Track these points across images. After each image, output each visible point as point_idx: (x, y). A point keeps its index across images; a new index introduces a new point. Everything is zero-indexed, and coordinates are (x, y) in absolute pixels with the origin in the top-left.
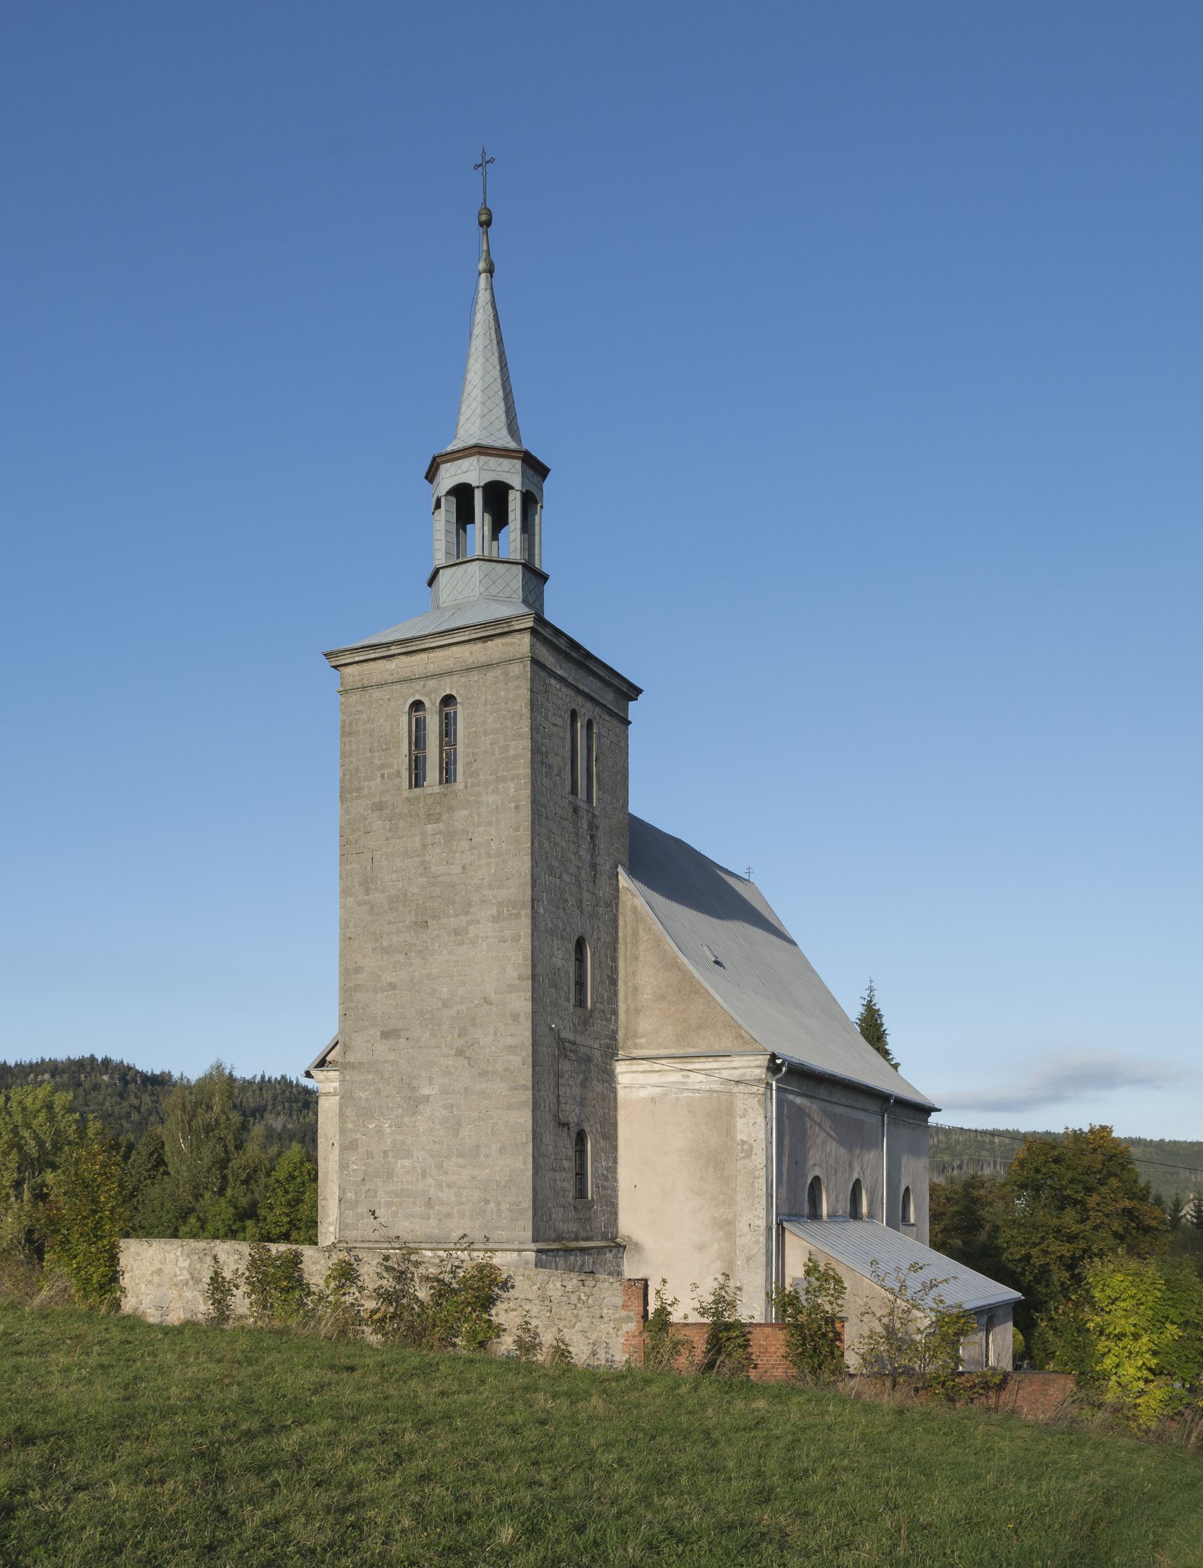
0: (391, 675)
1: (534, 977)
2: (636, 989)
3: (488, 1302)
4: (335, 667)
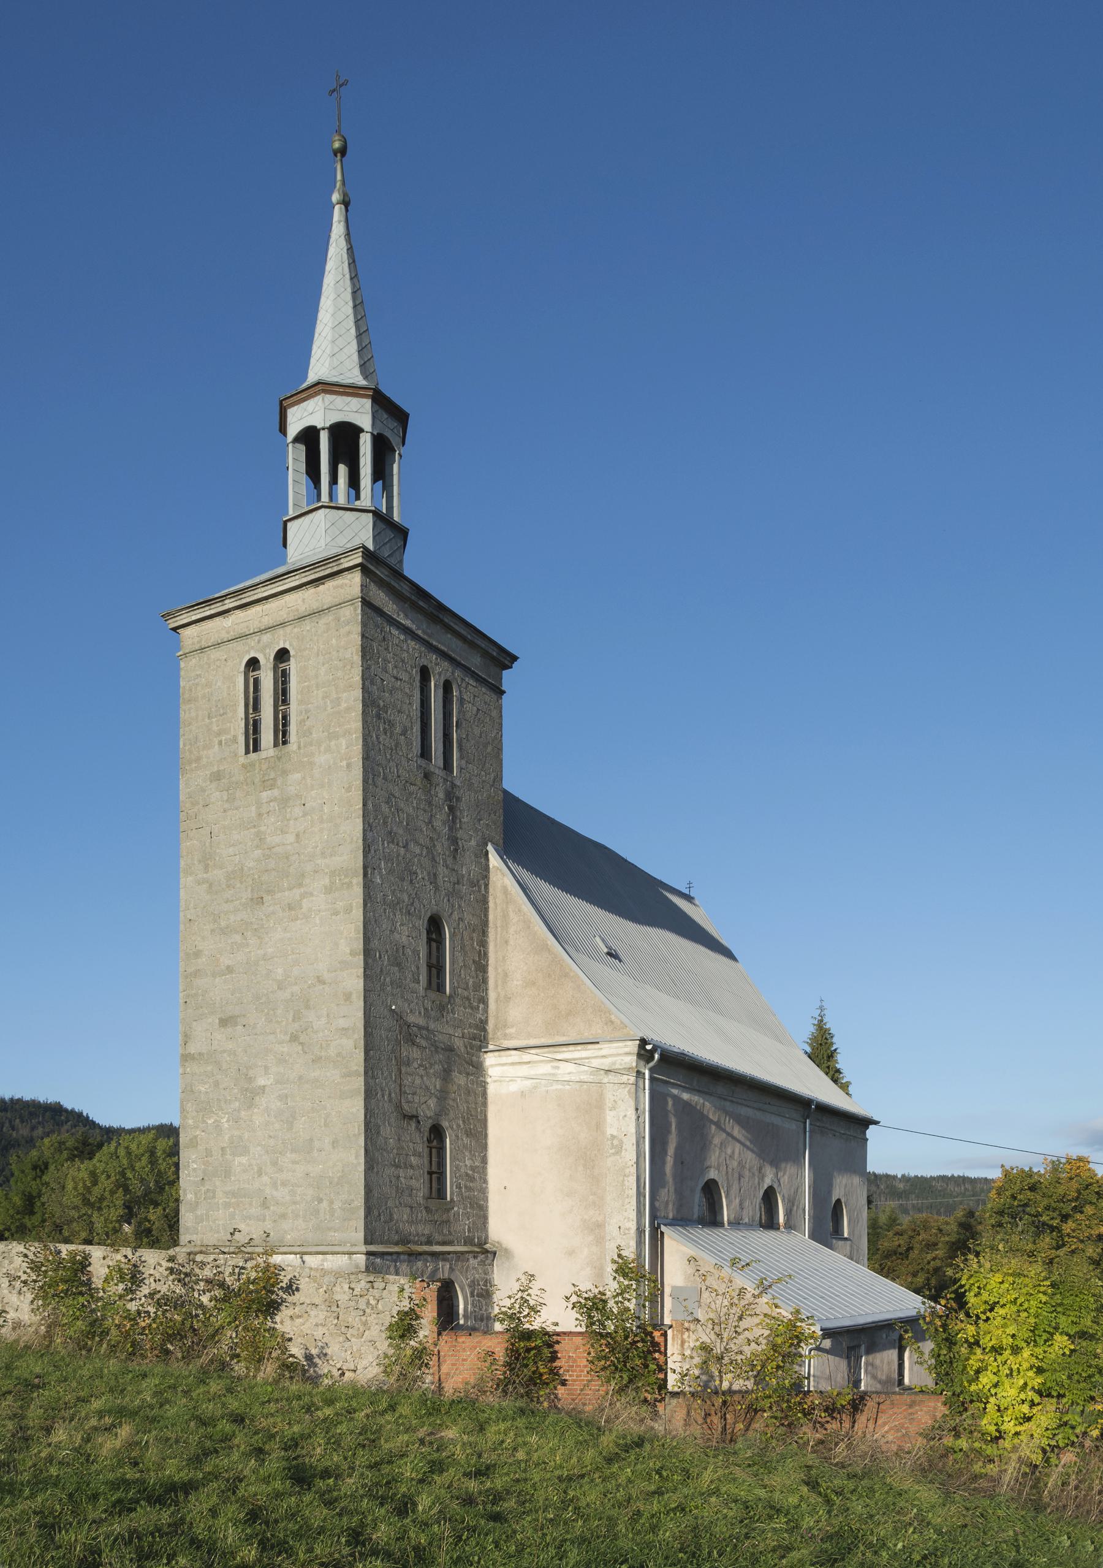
0: (228, 633)
1: (367, 952)
2: (506, 975)
3: (272, 1307)
4: (175, 629)
